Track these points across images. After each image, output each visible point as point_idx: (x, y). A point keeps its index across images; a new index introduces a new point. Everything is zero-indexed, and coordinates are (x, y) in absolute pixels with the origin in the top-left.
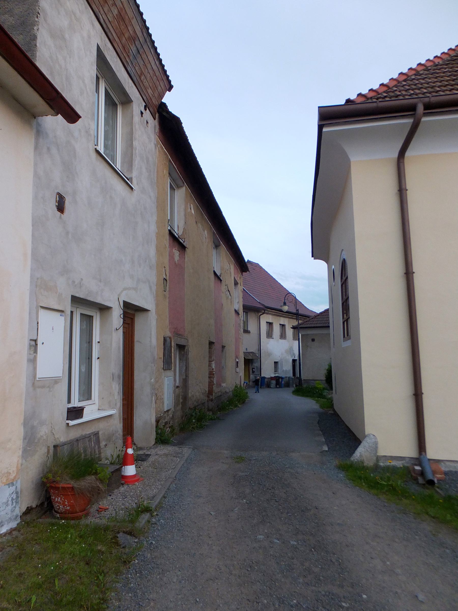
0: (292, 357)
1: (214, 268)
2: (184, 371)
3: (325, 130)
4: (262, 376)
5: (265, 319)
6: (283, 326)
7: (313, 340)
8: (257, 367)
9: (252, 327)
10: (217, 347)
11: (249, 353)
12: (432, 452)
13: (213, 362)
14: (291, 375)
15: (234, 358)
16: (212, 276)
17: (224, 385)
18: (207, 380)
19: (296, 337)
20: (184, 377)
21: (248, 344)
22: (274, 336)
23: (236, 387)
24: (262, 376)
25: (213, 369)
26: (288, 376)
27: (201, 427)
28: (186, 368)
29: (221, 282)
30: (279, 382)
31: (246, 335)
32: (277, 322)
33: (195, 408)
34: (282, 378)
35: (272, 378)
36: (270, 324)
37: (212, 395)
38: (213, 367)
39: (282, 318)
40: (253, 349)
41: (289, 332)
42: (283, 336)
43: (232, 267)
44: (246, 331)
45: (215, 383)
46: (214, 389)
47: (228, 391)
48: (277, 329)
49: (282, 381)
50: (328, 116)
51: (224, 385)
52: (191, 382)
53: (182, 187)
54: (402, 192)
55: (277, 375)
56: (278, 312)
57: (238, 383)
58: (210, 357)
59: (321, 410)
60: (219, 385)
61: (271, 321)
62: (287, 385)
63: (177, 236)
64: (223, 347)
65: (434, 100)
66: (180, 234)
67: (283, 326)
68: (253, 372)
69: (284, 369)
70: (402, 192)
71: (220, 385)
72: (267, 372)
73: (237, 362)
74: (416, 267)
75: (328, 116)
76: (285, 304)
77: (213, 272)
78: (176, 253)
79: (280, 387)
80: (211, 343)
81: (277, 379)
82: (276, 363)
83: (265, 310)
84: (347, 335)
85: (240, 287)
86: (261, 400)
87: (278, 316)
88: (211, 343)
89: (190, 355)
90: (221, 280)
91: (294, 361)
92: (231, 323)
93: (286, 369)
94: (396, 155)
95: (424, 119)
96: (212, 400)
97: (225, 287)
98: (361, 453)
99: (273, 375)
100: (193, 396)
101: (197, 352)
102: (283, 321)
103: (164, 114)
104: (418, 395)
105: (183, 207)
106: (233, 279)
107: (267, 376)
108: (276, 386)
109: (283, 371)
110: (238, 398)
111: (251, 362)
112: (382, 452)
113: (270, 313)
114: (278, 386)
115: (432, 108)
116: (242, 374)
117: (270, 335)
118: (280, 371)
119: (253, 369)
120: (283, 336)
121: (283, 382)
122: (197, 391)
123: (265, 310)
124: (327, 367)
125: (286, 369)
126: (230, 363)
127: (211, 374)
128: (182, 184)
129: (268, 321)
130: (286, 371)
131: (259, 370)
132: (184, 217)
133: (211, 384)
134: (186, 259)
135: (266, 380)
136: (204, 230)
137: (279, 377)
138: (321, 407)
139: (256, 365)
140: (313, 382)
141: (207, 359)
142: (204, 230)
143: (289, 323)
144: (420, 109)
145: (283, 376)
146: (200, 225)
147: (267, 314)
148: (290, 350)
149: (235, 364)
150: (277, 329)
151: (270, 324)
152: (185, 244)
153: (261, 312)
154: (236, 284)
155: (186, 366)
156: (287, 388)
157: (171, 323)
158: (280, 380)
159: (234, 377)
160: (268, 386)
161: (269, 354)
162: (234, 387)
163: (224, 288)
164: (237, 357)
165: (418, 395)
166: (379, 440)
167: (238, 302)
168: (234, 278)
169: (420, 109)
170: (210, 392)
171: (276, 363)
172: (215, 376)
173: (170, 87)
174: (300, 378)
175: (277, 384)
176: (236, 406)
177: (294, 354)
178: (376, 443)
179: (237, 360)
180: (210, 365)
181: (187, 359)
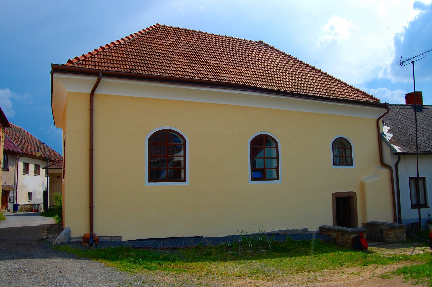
7: (58, 177)
30: (32, 210)
42: (37, 173)
48: (32, 167)
54: (91, 110)
70: (91, 110)
82: (30, 194)
91: (44, 192)
93: (39, 198)
104: (91, 207)
109: (36, 199)
117: (26, 171)
150: (32, 167)
161: (24, 187)
165: (91, 207)
171: (30, 194)
178: (70, 231)
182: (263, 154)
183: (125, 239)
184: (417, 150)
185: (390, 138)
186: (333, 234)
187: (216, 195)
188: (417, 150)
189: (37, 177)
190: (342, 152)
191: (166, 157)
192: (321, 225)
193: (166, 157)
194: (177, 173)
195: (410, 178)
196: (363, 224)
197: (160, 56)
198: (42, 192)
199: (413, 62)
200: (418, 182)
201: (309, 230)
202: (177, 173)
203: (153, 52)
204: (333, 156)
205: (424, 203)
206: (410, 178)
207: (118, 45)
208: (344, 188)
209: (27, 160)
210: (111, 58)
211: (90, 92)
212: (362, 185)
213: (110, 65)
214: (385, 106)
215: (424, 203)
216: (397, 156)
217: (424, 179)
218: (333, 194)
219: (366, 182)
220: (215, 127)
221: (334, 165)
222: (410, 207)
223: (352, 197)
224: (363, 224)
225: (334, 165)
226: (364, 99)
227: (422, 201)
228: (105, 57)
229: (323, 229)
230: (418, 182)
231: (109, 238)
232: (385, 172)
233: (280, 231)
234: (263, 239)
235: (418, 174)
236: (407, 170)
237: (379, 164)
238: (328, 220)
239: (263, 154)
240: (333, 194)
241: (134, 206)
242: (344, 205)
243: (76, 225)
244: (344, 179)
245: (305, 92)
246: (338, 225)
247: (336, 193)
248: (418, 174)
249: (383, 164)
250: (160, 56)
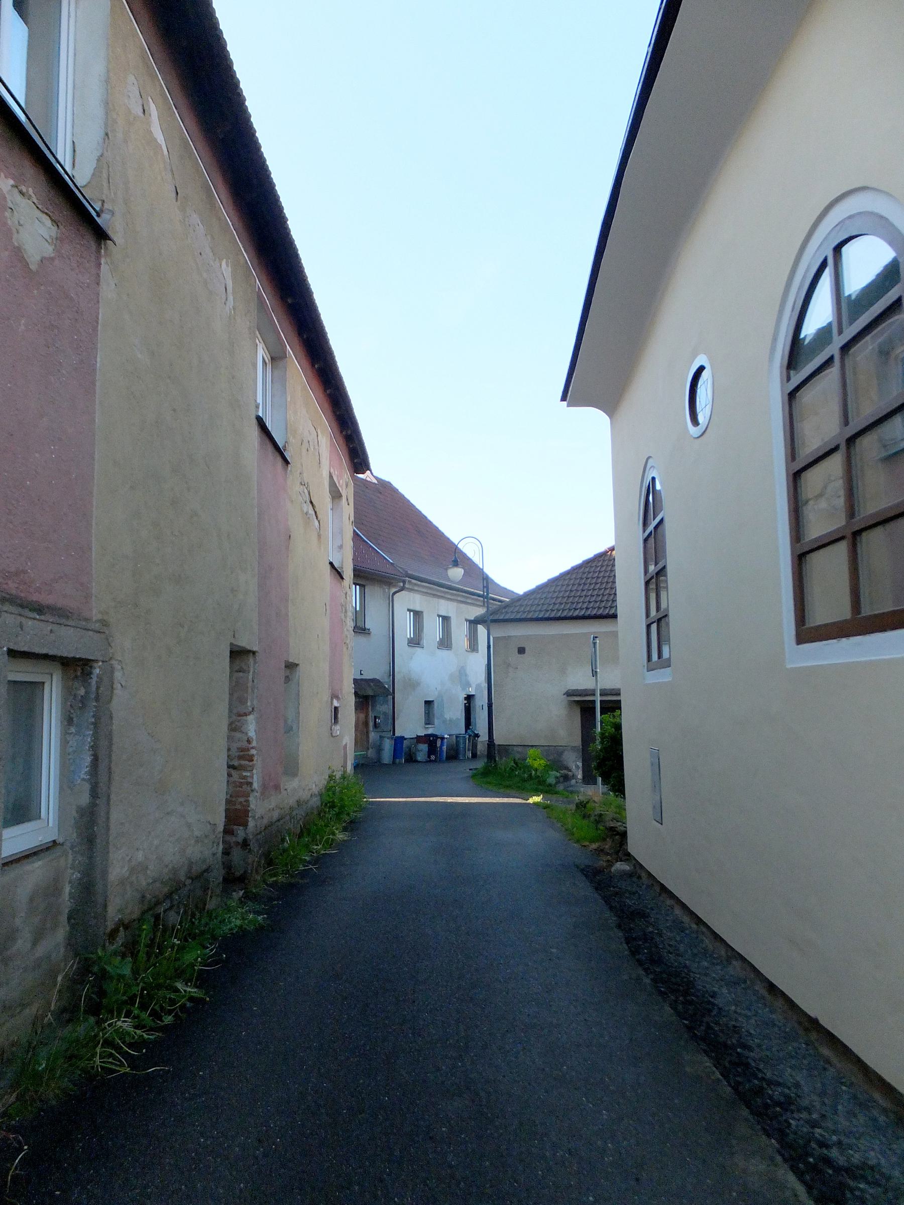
0: (463, 689)
1: (257, 407)
2: (84, 772)
4: (398, 733)
7: (521, 651)
8: (385, 714)
10: (264, 670)
11: (367, 681)
13: (251, 718)
14: (462, 730)
15: (326, 697)
16: (254, 432)
17: (294, 784)
24: (398, 733)
25: (249, 741)
26: (455, 732)
28: (96, 759)
29: (286, 469)
31: (362, 639)
32: (435, 608)
35: (419, 739)
37: (245, 825)
38: (252, 734)
39: (442, 601)
40: (376, 671)
44: (361, 630)
45: (255, 785)
46: (252, 806)
48: (433, 630)
49: (442, 744)
55: (430, 732)
57: (337, 765)
60: (272, 786)
61: (418, 609)
62: (454, 755)
63: (22, 117)
64: (291, 666)
68: (376, 725)
69: (447, 716)
72: (410, 725)
73: (336, 708)
77: (255, 421)
79: (438, 761)
80: (238, 654)
81: (431, 741)
82: (428, 703)
83: (404, 582)
87: (434, 595)
88: (238, 654)
89: (121, 703)
91: (469, 698)
97: (298, 488)
99: (422, 733)
102: (447, 607)
105: (98, 68)
106: (325, 474)
107: (407, 735)
108: (429, 757)
113: (416, 588)
114: (433, 757)
119: (375, 718)
121: (445, 747)
126: (313, 711)
129: (411, 608)
130: (451, 720)
131: (390, 721)
132: (99, 112)
137: (435, 737)
139: (383, 708)
140: (520, 749)
143: (461, 614)
149: (328, 715)
150: (433, 630)
153: (395, 586)
155: (94, 748)
156: (453, 765)
161: (413, 684)
164: (334, 696)
167: (341, 547)
168: (331, 476)
170: (236, 816)
172: (258, 762)
179: (336, 703)
180: (234, 727)
189: (444, 653)
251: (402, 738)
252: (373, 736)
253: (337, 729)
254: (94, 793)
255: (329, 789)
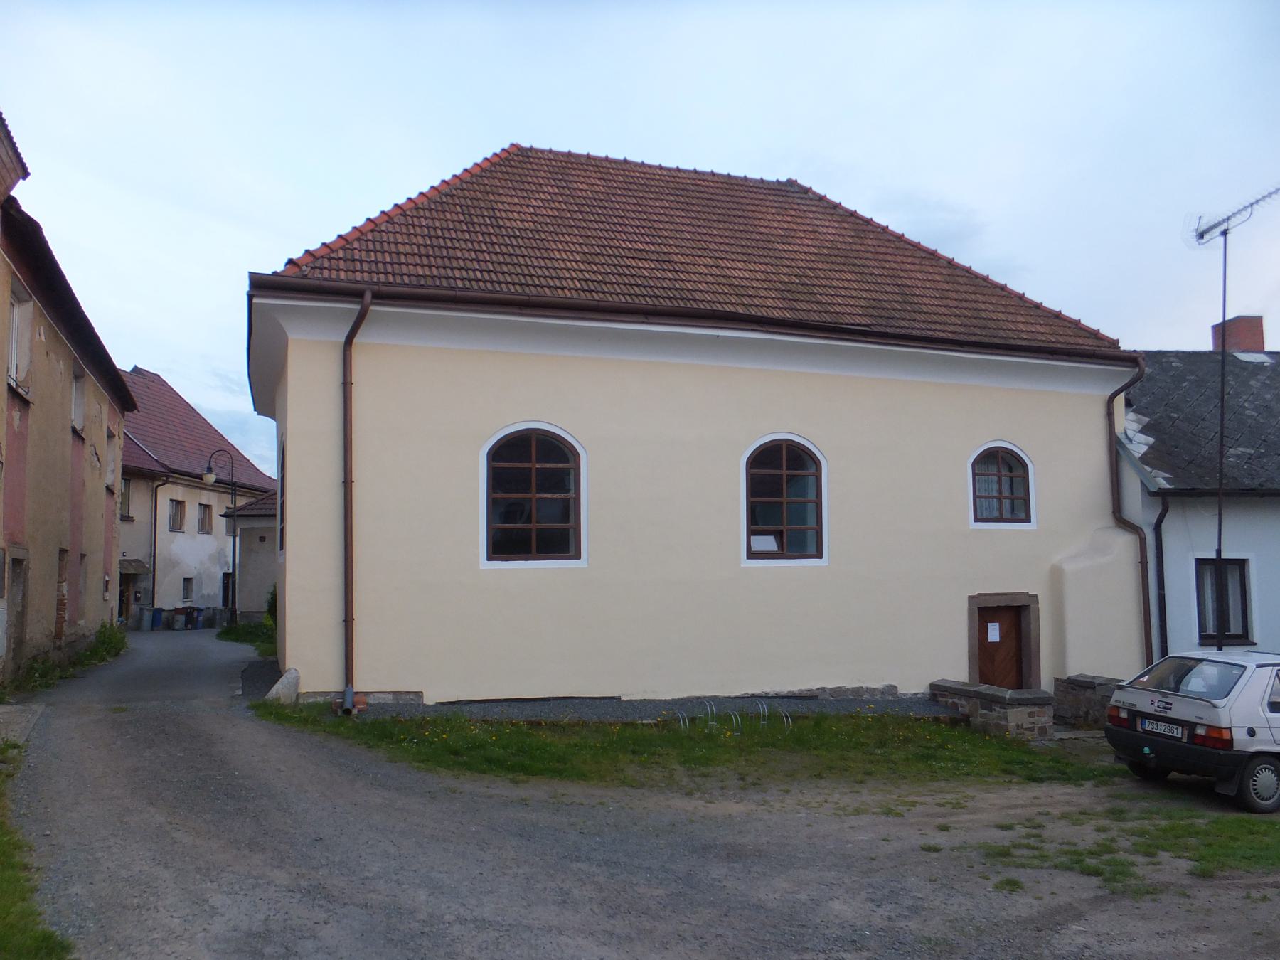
3: (255, 300)
4: (156, 606)
5: (167, 494)
6: (206, 508)
7: (262, 539)
9: (139, 508)
12: (360, 685)
14: (219, 602)
16: (69, 435)
17: (81, 622)
18: (53, 615)
19: (232, 532)
20: (20, 609)
21: (130, 543)
22: (185, 528)
23: (103, 626)
24: (156, 606)
27: (48, 686)
30: (191, 618)
31: (125, 527)
32: (193, 501)
33: (35, 658)
34: (199, 610)
35: (177, 611)
36: (179, 504)
39: (205, 492)
40: (140, 553)
41: (220, 524)
42: (205, 526)
43: (105, 408)
44: (126, 518)
47: (87, 633)
48: (192, 514)
50: (260, 285)
51: (81, 622)
52: (31, 615)
53: (26, 301)
54: (347, 385)
55: (188, 604)
56: (194, 480)
57: (107, 619)
58: (60, 575)
59: (260, 659)
60: (73, 623)
62: (210, 623)
64: (83, 556)
65: (384, 288)
66: (21, 378)
67: (206, 508)
68: (137, 599)
69: (205, 592)
70: (347, 385)
71: (75, 623)
72: (168, 597)
74: (356, 475)
75: (260, 285)
76: (210, 470)
78: (16, 414)
80: (63, 552)
82: (187, 581)
84: (282, 548)
85: (119, 442)
86: (149, 648)
88: (63, 552)
90: (83, 439)
91: (226, 576)
92: (98, 507)
93: (209, 594)
94: (342, 339)
95: (372, 308)
96: (59, 648)
98: (279, 690)
99: (180, 605)
100: (31, 639)
101: (40, 568)
102: (207, 497)
103: (12, 212)
104: (348, 622)
105: (27, 335)
106: (105, 429)
109: (202, 596)
110: (106, 646)
111: (134, 580)
112: (303, 689)
115: (380, 297)
116: (115, 603)
117: (176, 524)
118: (194, 596)
120: (205, 526)
122: (39, 630)
123: (168, 477)
124: (271, 589)
125: (209, 594)
126: (94, 583)
127: (61, 604)
128: (27, 297)
133: (60, 620)
134: (30, 422)
135: (164, 615)
136: (58, 361)
138: (260, 655)
139: (143, 585)
141: (56, 578)
142: (58, 361)
143: (219, 503)
144: (368, 296)
145: (202, 607)
146: (52, 355)
147: (172, 483)
148: (221, 552)
149: (102, 585)
150: (192, 514)
151: (179, 504)
152: (27, 397)
154: (111, 436)
157: (6, 527)
158: (195, 614)
159: (99, 607)
160: (169, 626)
161: (173, 564)
162: (98, 628)
163: (88, 450)
165: (348, 622)
166: (301, 674)
169: (368, 296)
170: (58, 635)
171: (187, 581)
173: (25, 174)
174: (233, 611)
175: (187, 623)
176: (103, 659)
177: (227, 563)
178: (297, 679)
181: (25, 581)
182: (782, 496)
183: (430, 699)
184: (1221, 484)
185: (1144, 449)
186: (963, 702)
187: (663, 603)
188: (1221, 484)
189: (204, 538)
190: (1002, 482)
191: (532, 498)
192: (934, 678)
193: (532, 498)
194: (557, 540)
195: (1200, 563)
196: (1057, 680)
197: (516, 237)
198: (220, 576)
199: (1225, 233)
200: (1222, 576)
201: (902, 690)
202: (557, 540)
203: (500, 227)
204: (975, 497)
205: (1240, 632)
206: (1200, 563)
207: (411, 210)
208: (1004, 583)
209: (178, 492)
210: (393, 248)
211: (343, 340)
212: (1056, 576)
213: (389, 268)
214: (1132, 359)
215: (1240, 632)
216: (1159, 500)
217: (1242, 564)
218: (971, 598)
219: (1068, 568)
220: (660, 423)
221: (976, 520)
222: (1197, 640)
223: (1027, 607)
224: (1057, 680)
225: (976, 520)
226: (1071, 340)
227: (1235, 628)
228: (378, 247)
229: (938, 691)
230: (1222, 576)
231: (391, 697)
232: (1124, 544)
233: (823, 689)
234: (769, 705)
235: (1219, 552)
236: (1190, 541)
237: (1108, 520)
238: (955, 666)
239: (782, 496)
240: (971, 598)
241: (424, 611)
242: (1006, 629)
243: (309, 664)
244: (1007, 559)
245: (903, 326)
246: (984, 679)
247: (980, 595)
248: (1219, 552)
249: (1121, 520)
250: (516, 237)
251: (160, 610)
252: (134, 608)
253: (107, 596)
254: (24, 607)
255: (100, 632)
